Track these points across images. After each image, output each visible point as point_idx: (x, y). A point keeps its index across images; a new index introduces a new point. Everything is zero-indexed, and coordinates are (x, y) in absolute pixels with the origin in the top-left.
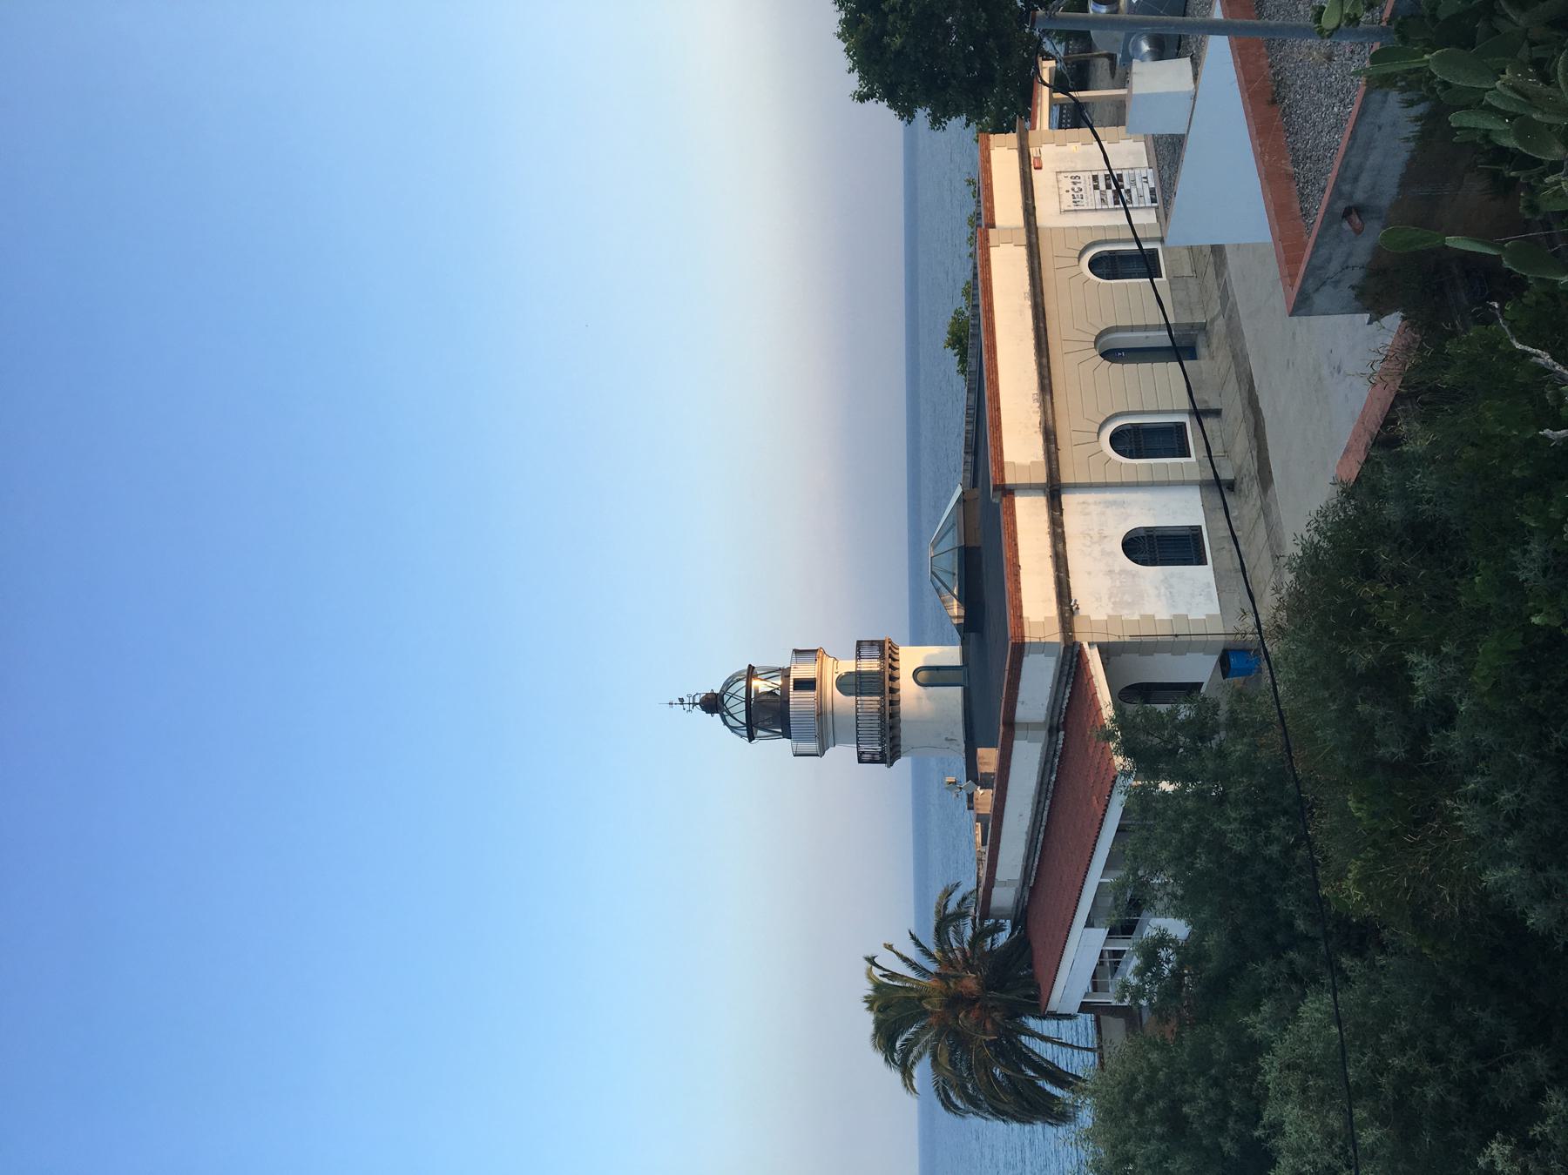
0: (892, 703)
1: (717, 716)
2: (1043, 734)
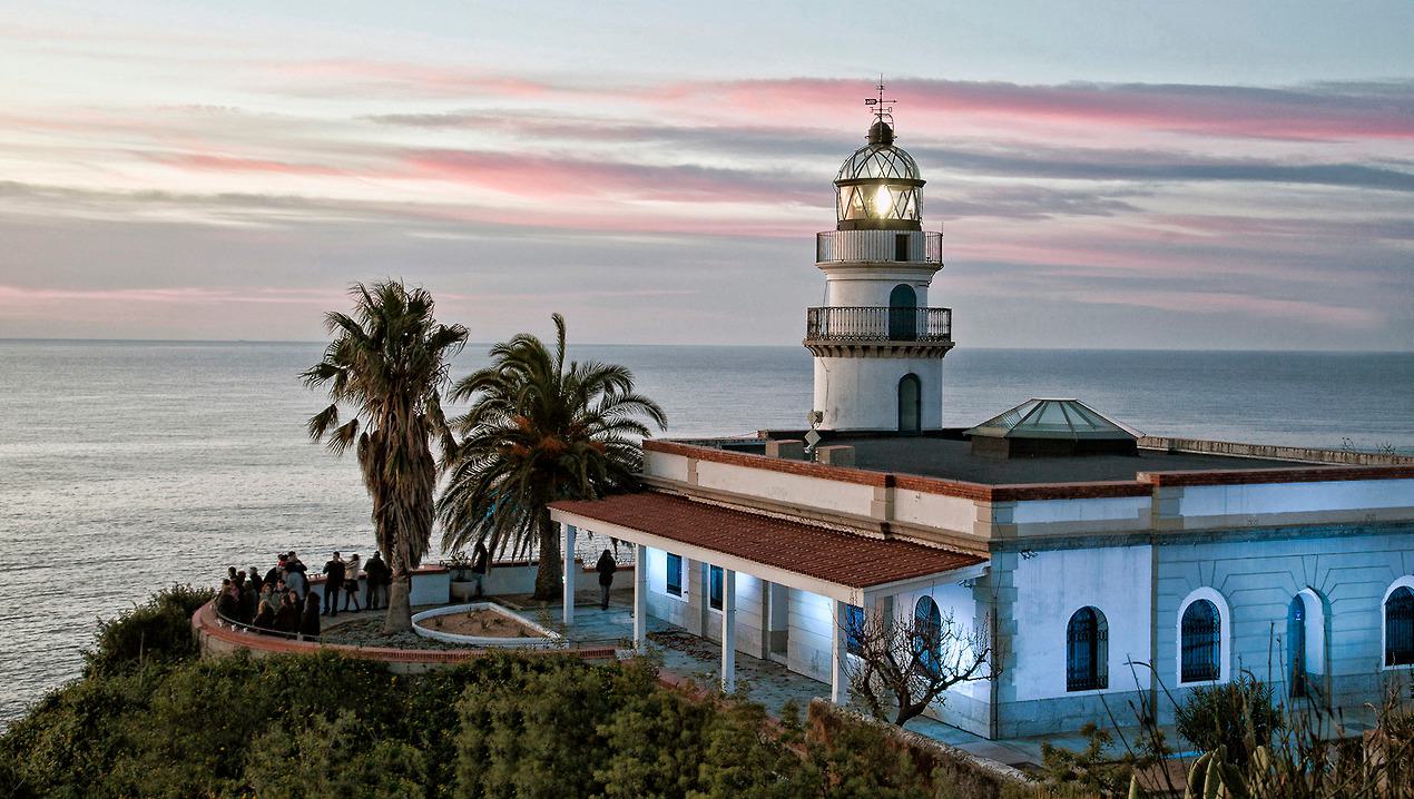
0: (880, 349)
1: (867, 142)
2: (882, 518)
